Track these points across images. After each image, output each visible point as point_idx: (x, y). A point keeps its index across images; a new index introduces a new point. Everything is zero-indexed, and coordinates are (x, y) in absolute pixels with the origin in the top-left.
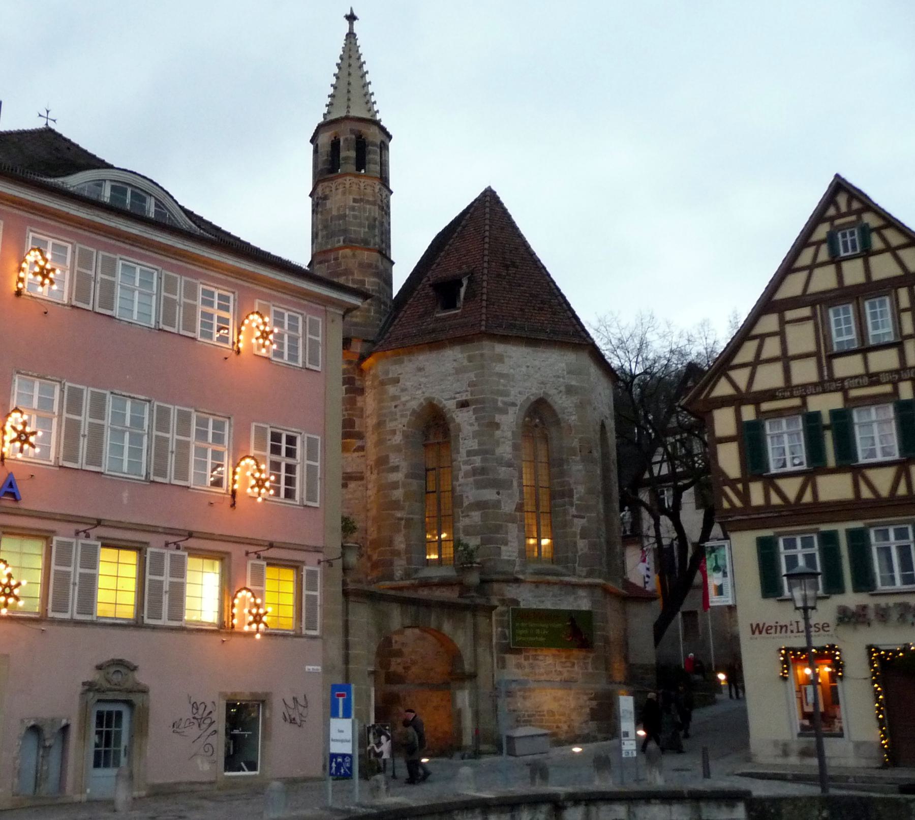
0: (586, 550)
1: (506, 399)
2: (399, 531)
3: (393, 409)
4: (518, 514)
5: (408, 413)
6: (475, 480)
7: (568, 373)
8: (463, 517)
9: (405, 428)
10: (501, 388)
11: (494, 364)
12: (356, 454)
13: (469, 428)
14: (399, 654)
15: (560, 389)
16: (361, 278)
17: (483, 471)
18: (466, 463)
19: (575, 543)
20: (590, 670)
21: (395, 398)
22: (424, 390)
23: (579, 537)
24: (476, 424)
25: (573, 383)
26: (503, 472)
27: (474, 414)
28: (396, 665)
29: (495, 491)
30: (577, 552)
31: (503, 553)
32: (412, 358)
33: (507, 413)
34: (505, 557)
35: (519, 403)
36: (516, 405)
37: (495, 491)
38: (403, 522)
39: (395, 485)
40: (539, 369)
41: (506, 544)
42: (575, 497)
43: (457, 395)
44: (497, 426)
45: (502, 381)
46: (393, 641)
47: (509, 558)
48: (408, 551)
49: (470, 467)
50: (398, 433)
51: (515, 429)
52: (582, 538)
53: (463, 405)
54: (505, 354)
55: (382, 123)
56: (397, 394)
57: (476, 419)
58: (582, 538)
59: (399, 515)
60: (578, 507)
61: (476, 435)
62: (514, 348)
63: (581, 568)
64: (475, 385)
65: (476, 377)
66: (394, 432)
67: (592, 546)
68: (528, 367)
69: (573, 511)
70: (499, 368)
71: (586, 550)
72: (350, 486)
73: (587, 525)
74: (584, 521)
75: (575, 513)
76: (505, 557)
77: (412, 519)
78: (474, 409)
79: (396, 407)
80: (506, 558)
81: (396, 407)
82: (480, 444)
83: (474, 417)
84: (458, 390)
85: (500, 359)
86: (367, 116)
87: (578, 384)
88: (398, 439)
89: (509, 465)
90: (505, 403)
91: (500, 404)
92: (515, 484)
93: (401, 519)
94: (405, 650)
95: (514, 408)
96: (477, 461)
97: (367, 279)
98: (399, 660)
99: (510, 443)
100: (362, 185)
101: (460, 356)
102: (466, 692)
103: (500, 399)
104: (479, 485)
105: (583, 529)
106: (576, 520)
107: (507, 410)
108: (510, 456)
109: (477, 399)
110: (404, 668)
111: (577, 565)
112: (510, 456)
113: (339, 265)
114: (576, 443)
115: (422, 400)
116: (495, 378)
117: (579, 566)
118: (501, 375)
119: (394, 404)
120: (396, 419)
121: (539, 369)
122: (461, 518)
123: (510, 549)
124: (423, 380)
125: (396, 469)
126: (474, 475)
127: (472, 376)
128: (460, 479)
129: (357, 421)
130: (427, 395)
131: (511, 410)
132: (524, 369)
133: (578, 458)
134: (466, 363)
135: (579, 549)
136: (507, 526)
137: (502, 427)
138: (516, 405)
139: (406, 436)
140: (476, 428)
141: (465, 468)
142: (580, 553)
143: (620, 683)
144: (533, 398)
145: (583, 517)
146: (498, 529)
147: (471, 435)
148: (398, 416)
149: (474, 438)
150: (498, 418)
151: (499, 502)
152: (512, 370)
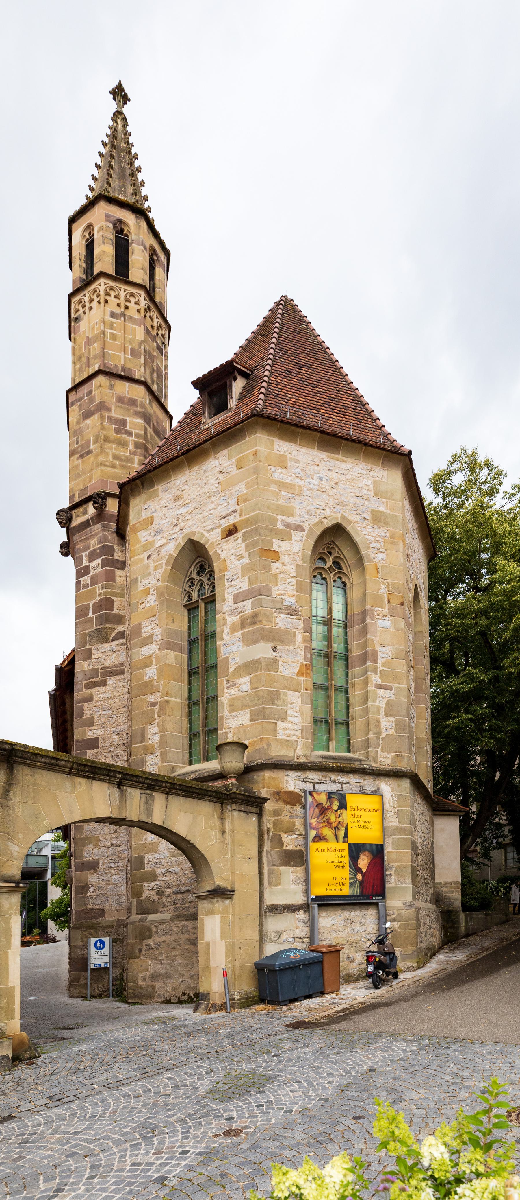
0: (392, 731)
1: (289, 520)
2: (152, 721)
3: (146, 561)
4: (302, 678)
5: (164, 561)
6: (243, 635)
7: (376, 495)
8: (228, 688)
9: (160, 584)
10: (282, 502)
11: (273, 469)
12: (116, 642)
13: (237, 562)
14: (153, 876)
15: (365, 515)
16: (121, 417)
17: (254, 619)
18: (232, 612)
19: (378, 721)
20: (100, 671)
21: (148, 545)
22: (182, 525)
23: (382, 714)
24: (246, 555)
25: (382, 509)
26: (283, 621)
27: (244, 541)
28: (149, 890)
29: (270, 645)
30: (380, 733)
31: (280, 732)
32: (168, 485)
33: (290, 539)
34: (281, 735)
35: (306, 526)
36: (303, 530)
37: (270, 645)
38: (156, 708)
39: (147, 663)
40: (336, 483)
41: (285, 720)
42: (379, 661)
43: (223, 521)
44: (275, 555)
45: (283, 493)
46: (146, 862)
47: (288, 738)
48: (163, 744)
49: (238, 617)
50: (151, 591)
51: (300, 563)
52: (387, 715)
53: (231, 532)
54: (289, 456)
55: (151, 215)
56: (151, 539)
57: (247, 546)
58: (387, 715)
59: (152, 698)
60: (383, 675)
61: (245, 570)
62: (304, 450)
63: (384, 754)
64: (245, 500)
65: (247, 489)
66: (147, 592)
67: (399, 726)
68: (321, 478)
69: (375, 679)
70: (278, 474)
71: (392, 731)
72: (109, 682)
73: (393, 698)
74: (388, 693)
75: (379, 682)
76: (281, 735)
77: (167, 702)
78: (244, 534)
79: (149, 557)
80: (283, 737)
81: (149, 557)
82: (250, 582)
83: (243, 545)
84: (224, 514)
85: (282, 462)
86: (131, 200)
87: (388, 511)
88: (151, 600)
89: (292, 612)
90: (288, 525)
91: (280, 526)
92: (299, 638)
93: (154, 704)
94: (159, 871)
95: (301, 534)
96: (247, 607)
97: (128, 419)
98: (152, 884)
99: (294, 581)
100: (122, 294)
101: (227, 464)
102: (217, 918)
103: (280, 518)
104: (249, 641)
105: (389, 704)
106: (381, 692)
107: (290, 534)
108: (293, 600)
109: (248, 519)
110: (158, 893)
111: (379, 750)
112: (293, 600)
113: (91, 400)
114: (383, 591)
115: (180, 540)
116: (274, 488)
117: (382, 751)
118: (282, 485)
119: (146, 554)
120: (150, 574)
121: (336, 483)
122: (226, 690)
123: (290, 726)
124: (183, 511)
125: (148, 640)
126: (243, 626)
127: (241, 488)
128: (225, 637)
129: (117, 602)
130: (186, 531)
131: (296, 536)
132: (316, 481)
133: (385, 611)
134: (234, 471)
135: (383, 730)
136: (286, 694)
137: (282, 558)
138: (303, 530)
139: (160, 594)
140: (246, 560)
141: (232, 619)
142: (384, 735)
143: (27, 862)
144: (327, 523)
145: (389, 689)
146: (274, 697)
147: (239, 570)
148: (152, 569)
149: (243, 576)
150: (276, 545)
151: (275, 660)
152: (298, 480)
